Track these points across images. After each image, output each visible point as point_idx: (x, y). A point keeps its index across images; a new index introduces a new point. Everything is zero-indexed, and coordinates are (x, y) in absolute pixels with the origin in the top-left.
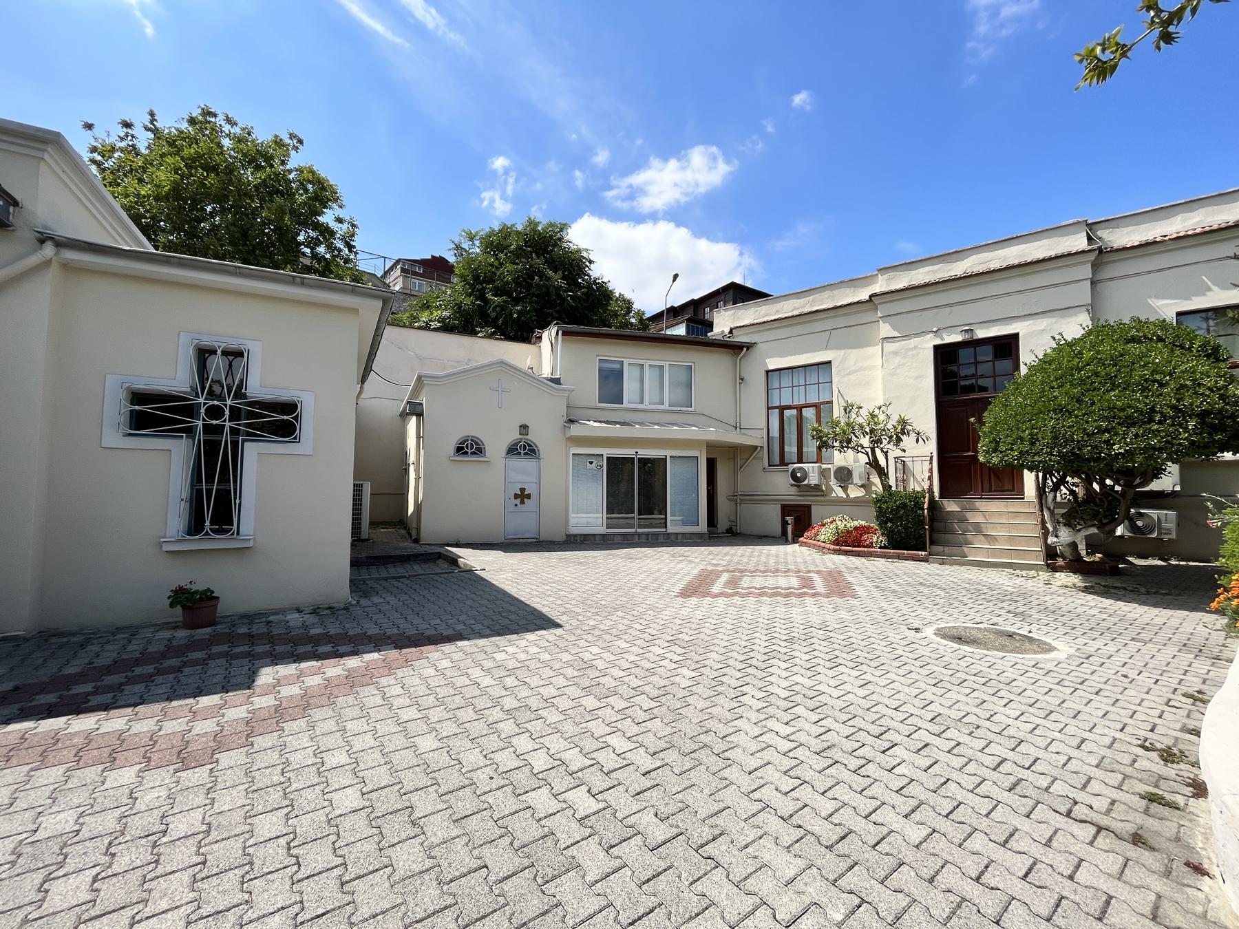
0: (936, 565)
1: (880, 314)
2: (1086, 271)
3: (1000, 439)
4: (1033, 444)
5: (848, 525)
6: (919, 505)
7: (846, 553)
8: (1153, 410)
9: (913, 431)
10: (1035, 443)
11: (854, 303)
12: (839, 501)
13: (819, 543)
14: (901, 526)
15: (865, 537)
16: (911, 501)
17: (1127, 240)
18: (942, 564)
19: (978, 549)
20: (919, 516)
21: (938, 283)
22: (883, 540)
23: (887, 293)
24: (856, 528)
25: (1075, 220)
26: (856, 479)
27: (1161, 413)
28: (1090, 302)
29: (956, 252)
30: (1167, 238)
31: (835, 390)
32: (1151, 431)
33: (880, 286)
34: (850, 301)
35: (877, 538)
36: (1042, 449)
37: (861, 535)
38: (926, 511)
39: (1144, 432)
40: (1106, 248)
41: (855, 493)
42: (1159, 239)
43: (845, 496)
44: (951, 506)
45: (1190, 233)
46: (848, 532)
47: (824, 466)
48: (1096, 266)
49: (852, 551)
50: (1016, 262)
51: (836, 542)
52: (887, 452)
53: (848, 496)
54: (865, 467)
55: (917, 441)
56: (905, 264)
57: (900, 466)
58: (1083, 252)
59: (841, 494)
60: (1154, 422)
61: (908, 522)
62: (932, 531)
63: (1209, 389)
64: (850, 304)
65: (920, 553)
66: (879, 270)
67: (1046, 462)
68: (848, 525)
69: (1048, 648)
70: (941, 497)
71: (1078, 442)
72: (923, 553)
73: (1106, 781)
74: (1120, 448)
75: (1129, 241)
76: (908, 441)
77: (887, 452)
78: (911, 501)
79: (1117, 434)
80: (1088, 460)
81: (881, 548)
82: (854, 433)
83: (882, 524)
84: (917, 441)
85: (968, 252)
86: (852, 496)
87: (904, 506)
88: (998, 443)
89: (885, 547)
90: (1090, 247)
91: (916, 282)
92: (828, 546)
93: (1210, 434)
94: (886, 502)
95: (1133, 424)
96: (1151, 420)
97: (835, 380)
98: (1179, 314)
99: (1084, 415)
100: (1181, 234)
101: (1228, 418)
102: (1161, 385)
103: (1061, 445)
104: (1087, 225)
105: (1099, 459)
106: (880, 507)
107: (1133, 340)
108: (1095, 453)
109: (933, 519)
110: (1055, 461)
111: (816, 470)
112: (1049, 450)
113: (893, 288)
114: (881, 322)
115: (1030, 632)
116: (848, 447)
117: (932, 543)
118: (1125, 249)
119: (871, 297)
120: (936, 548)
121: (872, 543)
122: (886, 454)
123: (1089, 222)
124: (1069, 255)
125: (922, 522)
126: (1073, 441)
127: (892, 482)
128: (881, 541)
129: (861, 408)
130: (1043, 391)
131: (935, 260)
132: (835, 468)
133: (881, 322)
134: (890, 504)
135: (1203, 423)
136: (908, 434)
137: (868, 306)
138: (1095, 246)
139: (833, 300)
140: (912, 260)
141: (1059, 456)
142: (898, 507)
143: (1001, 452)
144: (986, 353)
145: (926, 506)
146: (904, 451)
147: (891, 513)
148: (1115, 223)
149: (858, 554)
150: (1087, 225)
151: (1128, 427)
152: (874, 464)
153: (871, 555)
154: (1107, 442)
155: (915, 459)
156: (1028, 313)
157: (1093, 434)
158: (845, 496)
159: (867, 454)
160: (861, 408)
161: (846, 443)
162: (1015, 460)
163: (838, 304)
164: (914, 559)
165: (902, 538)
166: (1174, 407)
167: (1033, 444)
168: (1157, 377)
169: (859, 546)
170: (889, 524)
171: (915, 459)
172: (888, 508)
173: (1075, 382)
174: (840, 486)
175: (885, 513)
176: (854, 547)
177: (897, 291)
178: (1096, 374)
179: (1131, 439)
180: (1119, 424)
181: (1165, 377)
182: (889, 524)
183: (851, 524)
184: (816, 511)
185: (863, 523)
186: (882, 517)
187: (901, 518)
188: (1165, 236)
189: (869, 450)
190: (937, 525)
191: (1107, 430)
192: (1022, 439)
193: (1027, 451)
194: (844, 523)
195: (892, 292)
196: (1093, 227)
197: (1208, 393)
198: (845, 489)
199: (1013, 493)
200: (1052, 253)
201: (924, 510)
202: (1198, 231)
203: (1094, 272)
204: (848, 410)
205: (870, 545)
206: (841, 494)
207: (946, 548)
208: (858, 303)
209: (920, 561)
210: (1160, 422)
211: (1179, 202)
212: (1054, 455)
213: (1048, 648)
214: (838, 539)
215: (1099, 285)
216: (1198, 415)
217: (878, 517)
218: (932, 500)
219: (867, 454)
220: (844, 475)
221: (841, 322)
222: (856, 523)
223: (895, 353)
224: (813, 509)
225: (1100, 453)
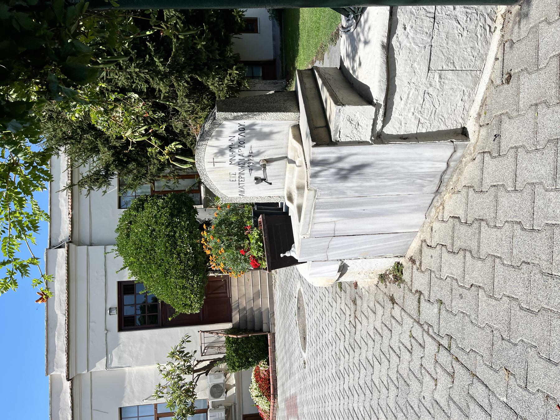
0: (276, 328)
1: (85, 372)
2: (82, 249)
3: (183, 303)
4: (186, 288)
5: (255, 387)
6: (235, 341)
7: (275, 389)
8: (168, 235)
9: (181, 345)
10: (185, 287)
11: (72, 393)
12: (239, 390)
13: (271, 410)
14: (250, 352)
15: (262, 376)
16: (232, 346)
17: (66, 230)
18: (274, 324)
19: (263, 303)
20: (242, 340)
21: (68, 332)
22: (262, 363)
23: (68, 368)
24: (257, 381)
25: (45, 254)
26: (221, 380)
27: (170, 232)
28: (103, 247)
29: (47, 321)
30: (71, 213)
31: (146, 402)
32: (180, 236)
33: (61, 372)
34: (69, 395)
35: (262, 366)
36: (190, 283)
37: (261, 378)
38: (238, 337)
39: (180, 239)
40: (69, 239)
41: (232, 379)
42: (70, 216)
43: (235, 388)
44: (236, 317)
45: (70, 204)
46: (260, 387)
47: (210, 407)
48: (80, 244)
49: (273, 385)
50: (65, 285)
51: (268, 396)
52: (197, 361)
53: (234, 385)
54: (211, 375)
55: (189, 341)
56: (47, 355)
57: (210, 350)
58: (68, 251)
59: (233, 391)
60: (174, 235)
61: (248, 347)
62: (253, 330)
63: (158, 212)
64: (72, 396)
65: (269, 338)
66: (47, 374)
67: (198, 282)
68: (255, 387)
69: (300, 291)
70: (230, 320)
71: (185, 267)
72: (269, 336)
73: (340, 302)
74: (189, 249)
75: (68, 229)
76: (188, 348)
77: (197, 361)
78: (232, 346)
79: (181, 250)
80: (196, 262)
81: (268, 364)
82: (181, 387)
83: (250, 364)
84: (189, 341)
85: (50, 346)
86: (234, 383)
87: (236, 351)
88: (186, 305)
89: (268, 361)
90: (66, 248)
91: (64, 347)
92: (272, 404)
93: (183, 213)
94: (234, 363)
95: (175, 243)
96: (174, 236)
97: (137, 403)
98: (120, 207)
99: (168, 264)
100: (70, 207)
101: (174, 206)
102: (154, 230)
103: (187, 275)
104: (50, 248)
105: (195, 257)
106: (238, 367)
107: (128, 236)
108: (192, 259)
109: (245, 331)
110: (197, 278)
111: (213, 414)
112: (190, 280)
113: (65, 362)
114: (93, 370)
115: (295, 297)
116: (193, 392)
117: (261, 330)
118: (72, 231)
119: (68, 379)
120: (265, 327)
121: (266, 371)
122: (199, 362)
123: (48, 247)
124: (68, 257)
125: (248, 337)
126: (185, 269)
127: (221, 356)
128: (264, 364)
129: (160, 385)
130: (153, 281)
131: (50, 335)
132: (212, 398)
133: (93, 370)
134: (235, 359)
135: (176, 216)
136: (184, 348)
137: (76, 382)
138: (66, 245)
139: (65, 410)
140: (45, 350)
141: (194, 276)
142: (237, 355)
143: (192, 302)
144: (128, 299)
145: (236, 337)
146: (195, 351)
147: (241, 359)
148: (51, 349)
149: (275, 380)
150: (50, 248)
151: (177, 245)
152: (207, 370)
153: (274, 371)
154: (185, 255)
155: (203, 342)
156: (104, 277)
157: (180, 260)
158: (235, 388)
159: (199, 375)
160: (160, 385)
161: (189, 392)
162: (197, 296)
163: (70, 405)
164: (274, 342)
165: (260, 350)
166: (167, 227)
167: (186, 288)
168: (149, 232)
169: (269, 380)
170: (250, 360)
171: (203, 342)
172: (238, 362)
173: (148, 266)
174: (226, 393)
175: (242, 363)
176: (270, 383)
177: (68, 360)
178: (145, 257)
179: (184, 244)
180: (175, 249)
181: (149, 229)
182: (250, 360)
183: (254, 385)
184: (247, 412)
185: (253, 375)
186: (247, 364)
187: (245, 352)
188: (69, 213)
189: (195, 375)
190: (249, 326)
191: (179, 254)
192: (183, 293)
193: (191, 291)
194: (254, 390)
195: (68, 364)
196: (52, 245)
197: (160, 213)
198: (228, 388)
199: (227, 281)
200: (64, 266)
201: (238, 338)
202: (70, 201)
203: (84, 245)
204: (161, 395)
205: (268, 371)
206: (233, 391)
207: (264, 322)
208: (71, 389)
209: (275, 338)
210: (175, 232)
211: (49, 230)
212: (193, 278)
213: (300, 291)
214: (266, 396)
215: (93, 242)
216: (172, 218)
217: (247, 368)
218: (234, 331)
219: (199, 375)
220: (216, 390)
221: (86, 402)
222: (253, 380)
223: (120, 358)
224: (244, 414)
225: (192, 257)
